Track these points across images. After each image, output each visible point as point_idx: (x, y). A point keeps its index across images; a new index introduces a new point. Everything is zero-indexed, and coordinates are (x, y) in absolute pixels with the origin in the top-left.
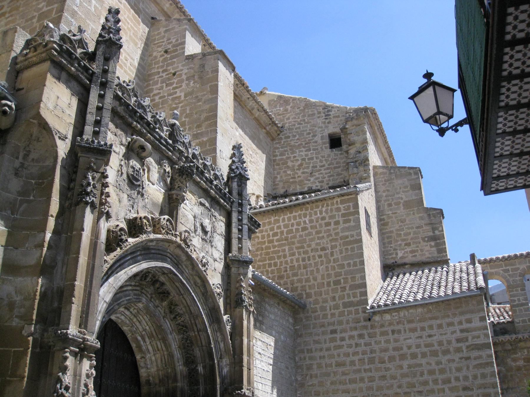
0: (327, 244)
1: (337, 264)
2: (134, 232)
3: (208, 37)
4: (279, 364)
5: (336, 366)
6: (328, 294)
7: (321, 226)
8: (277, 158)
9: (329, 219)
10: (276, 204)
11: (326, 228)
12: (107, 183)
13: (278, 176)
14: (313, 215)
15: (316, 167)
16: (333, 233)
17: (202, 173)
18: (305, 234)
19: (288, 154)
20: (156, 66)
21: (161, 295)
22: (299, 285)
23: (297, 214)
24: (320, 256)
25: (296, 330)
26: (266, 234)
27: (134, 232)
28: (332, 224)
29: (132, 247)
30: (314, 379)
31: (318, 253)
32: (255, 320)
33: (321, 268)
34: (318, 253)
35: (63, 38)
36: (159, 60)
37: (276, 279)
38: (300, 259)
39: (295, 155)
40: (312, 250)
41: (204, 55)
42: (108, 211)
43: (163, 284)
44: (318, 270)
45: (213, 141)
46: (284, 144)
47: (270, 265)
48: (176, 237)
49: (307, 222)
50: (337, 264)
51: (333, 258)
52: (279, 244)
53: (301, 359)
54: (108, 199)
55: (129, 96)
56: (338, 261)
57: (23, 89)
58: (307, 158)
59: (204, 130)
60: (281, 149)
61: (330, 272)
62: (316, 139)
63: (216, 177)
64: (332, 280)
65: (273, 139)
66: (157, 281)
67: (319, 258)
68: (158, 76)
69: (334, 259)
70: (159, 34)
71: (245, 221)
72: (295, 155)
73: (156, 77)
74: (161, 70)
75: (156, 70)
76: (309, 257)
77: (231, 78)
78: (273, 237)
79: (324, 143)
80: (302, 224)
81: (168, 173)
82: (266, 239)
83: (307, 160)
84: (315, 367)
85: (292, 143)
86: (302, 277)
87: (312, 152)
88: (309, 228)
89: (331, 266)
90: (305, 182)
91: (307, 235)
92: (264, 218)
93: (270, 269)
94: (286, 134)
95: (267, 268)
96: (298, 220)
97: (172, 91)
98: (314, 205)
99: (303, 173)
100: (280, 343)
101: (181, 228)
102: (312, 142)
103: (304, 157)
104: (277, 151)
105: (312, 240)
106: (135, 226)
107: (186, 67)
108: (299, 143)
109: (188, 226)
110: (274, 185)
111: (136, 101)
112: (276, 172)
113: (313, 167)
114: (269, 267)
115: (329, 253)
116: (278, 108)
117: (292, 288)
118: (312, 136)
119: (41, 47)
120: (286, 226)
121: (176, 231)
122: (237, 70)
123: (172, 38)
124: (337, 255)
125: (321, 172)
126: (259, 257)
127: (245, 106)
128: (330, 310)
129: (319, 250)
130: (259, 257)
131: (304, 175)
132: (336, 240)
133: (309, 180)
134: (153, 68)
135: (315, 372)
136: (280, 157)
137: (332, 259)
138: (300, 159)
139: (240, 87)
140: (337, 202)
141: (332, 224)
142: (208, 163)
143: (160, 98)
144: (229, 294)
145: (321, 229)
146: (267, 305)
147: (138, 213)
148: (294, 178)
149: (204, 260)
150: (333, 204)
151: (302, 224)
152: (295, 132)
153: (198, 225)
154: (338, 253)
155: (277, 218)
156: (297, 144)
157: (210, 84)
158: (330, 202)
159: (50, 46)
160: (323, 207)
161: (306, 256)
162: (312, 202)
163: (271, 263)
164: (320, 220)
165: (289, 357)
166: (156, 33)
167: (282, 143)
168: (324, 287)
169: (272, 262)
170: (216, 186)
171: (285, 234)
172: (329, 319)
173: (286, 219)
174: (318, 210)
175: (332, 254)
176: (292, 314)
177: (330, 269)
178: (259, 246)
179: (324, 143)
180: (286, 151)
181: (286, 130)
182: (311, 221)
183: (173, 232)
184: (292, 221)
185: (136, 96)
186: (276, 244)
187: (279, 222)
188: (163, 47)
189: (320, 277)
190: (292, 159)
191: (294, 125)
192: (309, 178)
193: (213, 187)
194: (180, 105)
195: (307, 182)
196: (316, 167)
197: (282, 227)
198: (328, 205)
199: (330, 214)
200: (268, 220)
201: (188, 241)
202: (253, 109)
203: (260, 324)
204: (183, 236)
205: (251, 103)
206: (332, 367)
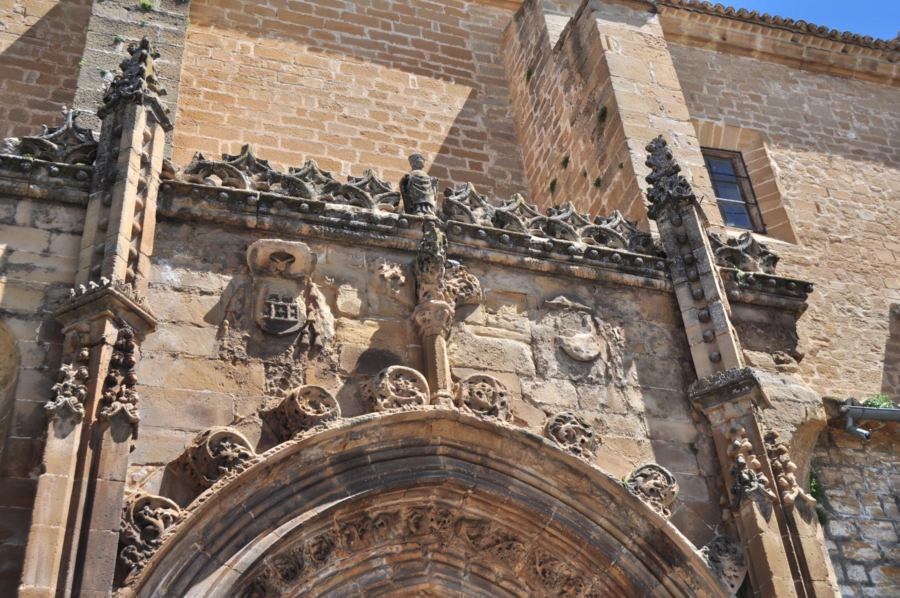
43: (480, 524)
74: (532, 109)
127: (850, 70)
202: (874, 65)
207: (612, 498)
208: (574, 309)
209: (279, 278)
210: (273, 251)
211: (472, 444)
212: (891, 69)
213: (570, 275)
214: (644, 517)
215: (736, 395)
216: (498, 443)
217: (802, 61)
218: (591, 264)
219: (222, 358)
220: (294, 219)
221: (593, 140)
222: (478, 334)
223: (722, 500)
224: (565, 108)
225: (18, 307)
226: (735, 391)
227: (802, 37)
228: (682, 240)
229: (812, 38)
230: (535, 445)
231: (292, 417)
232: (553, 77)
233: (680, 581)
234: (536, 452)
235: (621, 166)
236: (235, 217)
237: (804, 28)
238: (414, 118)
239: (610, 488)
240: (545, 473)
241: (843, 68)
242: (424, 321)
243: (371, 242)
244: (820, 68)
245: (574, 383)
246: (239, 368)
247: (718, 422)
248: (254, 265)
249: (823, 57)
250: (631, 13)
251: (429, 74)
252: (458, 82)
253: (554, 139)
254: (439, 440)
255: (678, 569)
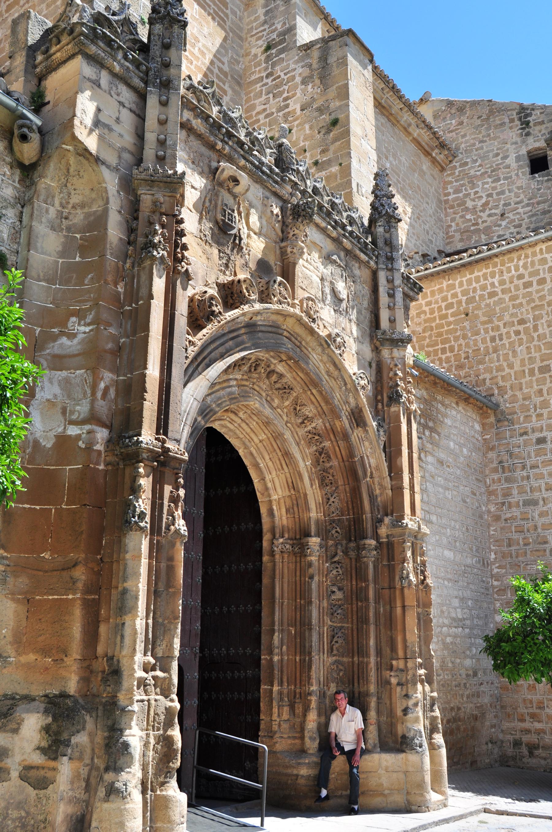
0: (528, 314)
1: (544, 342)
2: (231, 301)
3: (333, 15)
4: (461, 488)
5: (547, 490)
6: (532, 387)
7: (517, 288)
8: (450, 198)
9: (530, 277)
10: (448, 261)
11: (525, 291)
12: (182, 230)
13: (453, 224)
14: (505, 273)
15: (509, 204)
16: (535, 296)
17: (329, 214)
18: (494, 301)
19: (466, 190)
20: (257, 69)
21: (281, 392)
22: (488, 376)
23: (480, 274)
24: (517, 333)
25: (485, 439)
26: (436, 306)
27: (231, 301)
28: (535, 283)
29: (229, 322)
30: (514, 509)
31: (514, 328)
32: (423, 427)
33: (519, 350)
34: (514, 328)
35: (99, 18)
36: (261, 60)
37: (453, 370)
38: (488, 339)
39: (477, 190)
40: (505, 324)
41: (325, 41)
42: (187, 270)
43: (281, 376)
44: (514, 352)
45: (346, 171)
46: (458, 176)
47: (444, 351)
48: (295, 307)
49: (497, 284)
50: (544, 342)
51: (537, 334)
52: (456, 320)
53: (494, 482)
54: (186, 253)
55: (209, 104)
56: (546, 338)
57: (49, 102)
58: (494, 192)
59: (332, 156)
60: (455, 184)
61: (533, 354)
62: (507, 161)
63: (352, 222)
64: (536, 366)
65: (443, 169)
66: (273, 371)
67: (516, 335)
68: (261, 84)
69: (538, 336)
70: (256, 19)
71: (398, 281)
72: (477, 190)
73: (259, 85)
74: (264, 74)
75: (257, 76)
76: (501, 336)
77: (368, 73)
78: (446, 309)
79: (520, 167)
80: (489, 287)
81: (277, 215)
82: (436, 314)
83: (494, 196)
84: (515, 492)
85: (472, 172)
86: (492, 365)
87: (502, 182)
88: (500, 293)
89: (535, 346)
90: (494, 228)
91: (496, 303)
92: (433, 284)
93: (444, 357)
94: (462, 159)
95: (440, 355)
96: (482, 282)
97: (282, 104)
98: (506, 258)
99: (490, 215)
100: (462, 459)
101: (300, 294)
102: (501, 166)
103: (490, 192)
104: (449, 186)
105: (505, 309)
106: (232, 293)
107: (300, 64)
108: (483, 171)
109: (313, 292)
110: (447, 238)
111: (220, 112)
112: (449, 218)
113: (505, 205)
114: (442, 354)
115: (531, 326)
116: (449, 122)
117: (476, 381)
118: (502, 158)
119: (65, 35)
120: (464, 293)
121: (294, 298)
122: (378, 61)
123: (276, 22)
124: (543, 329)
125: (518, 211)
126: (428, 340)
127: (398, 121)
128: (535, 410)
129: (516, 323)
130: (428, 340)
131: (491, 218)
132: (541, 307)
133: (500, 226)
134: (253, 73)
135: (516, 500)
136: (454, 196)
137: (535, 335)
138: (484, 195)
139: (388, 93)
140: (541, 250)
141: (535, 283)
142: (337, 201)
143: (266, 117)
144: (379, 388)
145: (518, 293)
146: (440, 405)
147: (235, 275)
148: (477, 224)
149: (339, 339)
150: (534, 254)
151: (489, 287)
152: (475, 155)
153: (327, 290)
154: (545, 327)
155: (451, 282)
156: (478, 173)
157: (337, 85)
158: (529, 251)
159: (77, 30)
160: (519, 259)
161: (497, 334)
162: (503, 254)
163: (445, 348)
164: (515, 279)
165: (476, 479)
166: (252, 18)
167: (457, 174)
168: (525, 377)
169: (447, 346)
170: (351, 233)
171: (464, 304)
172: (534, 422)
173: (465, 283)
174: (512, 265)
175: (536, 328)
176: (478, 419)
177: (533, 350)
178: (428, 324)
179: (520, 167)
180: (462, 185)
181: (462, 153)
182: (502, 282)
183: (289, 300)
184: (474, 285)
185: (219, 104)
186: (451, 319)
187: (455, 288)
188: (264, 38)
189: (519, 362)
190: (472, 196)
191: (474, 145)
192: (499, 222)
193: (347, 234)
194: (296, 123)
195: (497, 228)
196: (509, 204)
197: (459, 295)
198: (527, 257)
199: (530, 270)
200: (438, 287)
201: (312, 312)
202: (410, 125)
203: (431, 432)
204: (305, 305)
205: (406, 117)
206: (541, 491)
207: (346, 384)
208: (340, 266)
209: (226, 192)
210: (231, 174)
211: (298, 335)
212: (415, 131)
213: (341, 243)
214: (356, 399)
215: (399, 346)
216: (309, 338)
217: (380, 104)
218: (351, 241)
219: (201, 239)
220: (238, 152)
221: (319, 132)
222: (303, 266)
223: (379, 397)
224: (298, 95)
225: (106, 158)
226: (400, 343)
227: (388, 89)
228: (388, 243)
229: (392, 93)
230: (326, 346)
231: (237, 294)
232: (292, 66)
233: (359, 435)
234: (323, 349)
235: (340, 164)
236: (212, 139)
237: (391, 85)
238: (193, 41)
239: (348, 380)
240: (321, 361)
241: (396, 119)
242: (291, 252)
243: (269, 185)
244: (385, 113)
245: (335, 310)
246: (207, 247)
247: (386, 356)
248: (219, 178)
249: (390, 107)
250: (362, 57)
251: (205, 10)
252: (219, 24)
253: (280, 109)
254: (285, 327)
255: (360, 429)
